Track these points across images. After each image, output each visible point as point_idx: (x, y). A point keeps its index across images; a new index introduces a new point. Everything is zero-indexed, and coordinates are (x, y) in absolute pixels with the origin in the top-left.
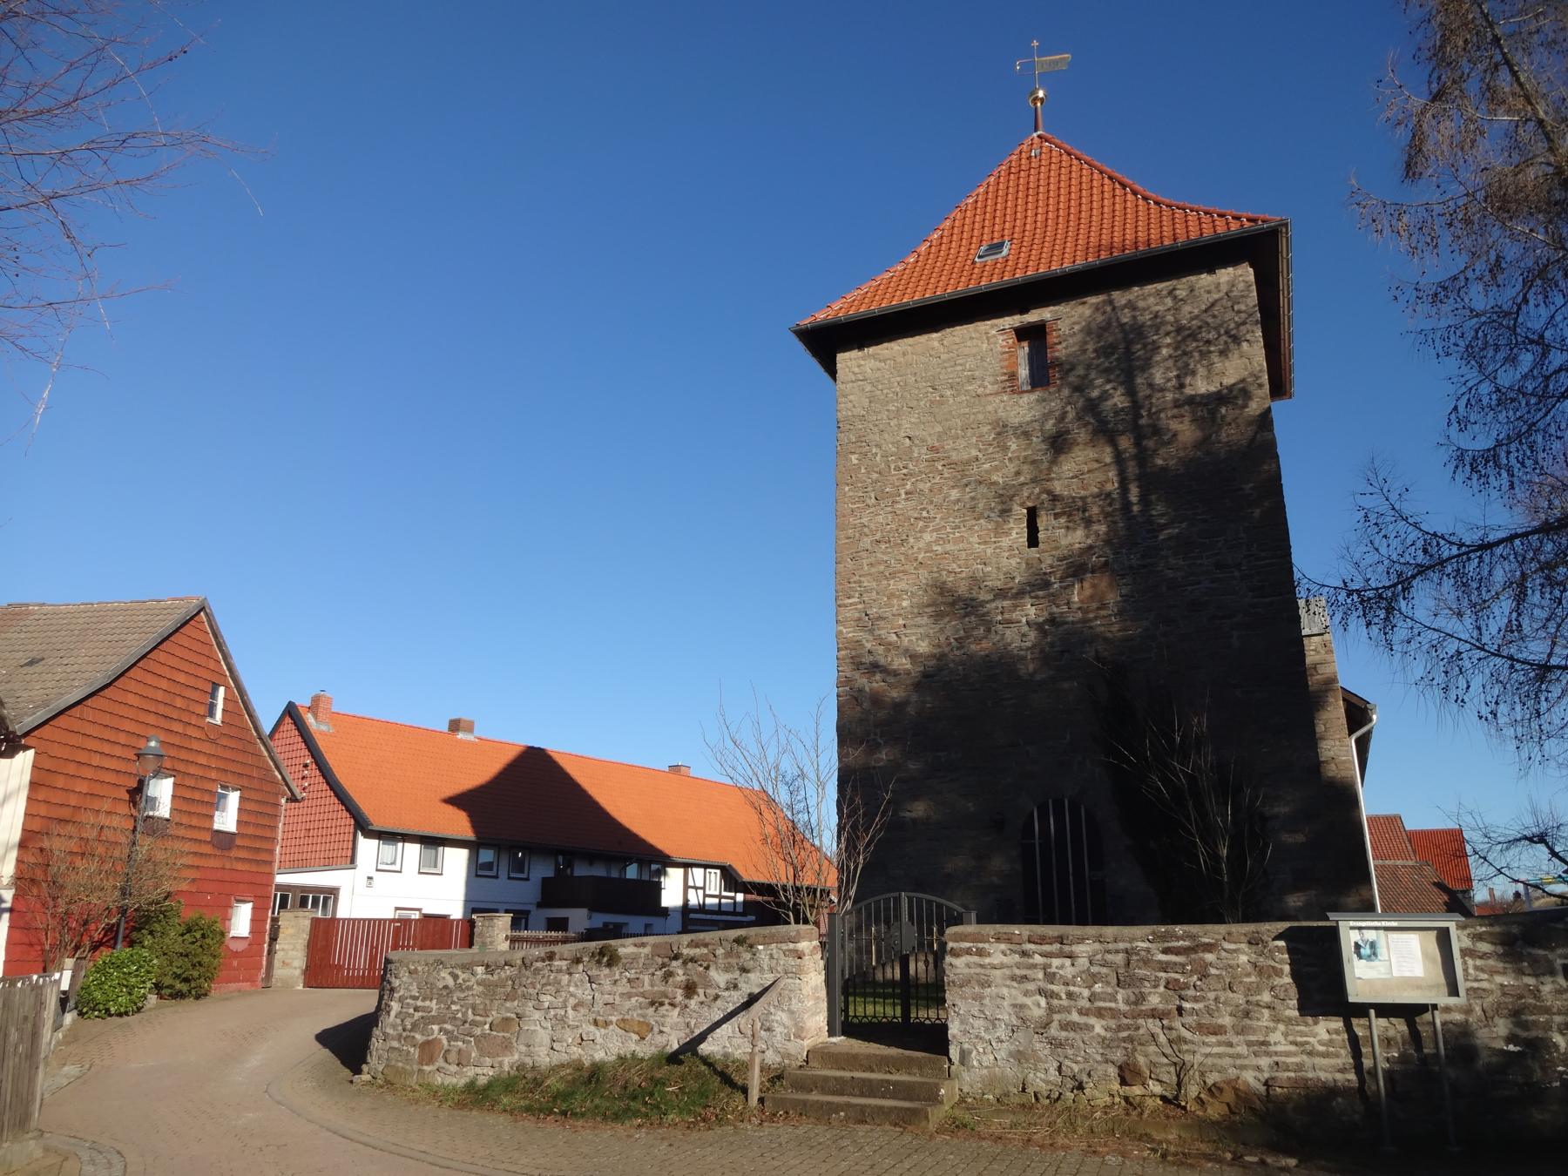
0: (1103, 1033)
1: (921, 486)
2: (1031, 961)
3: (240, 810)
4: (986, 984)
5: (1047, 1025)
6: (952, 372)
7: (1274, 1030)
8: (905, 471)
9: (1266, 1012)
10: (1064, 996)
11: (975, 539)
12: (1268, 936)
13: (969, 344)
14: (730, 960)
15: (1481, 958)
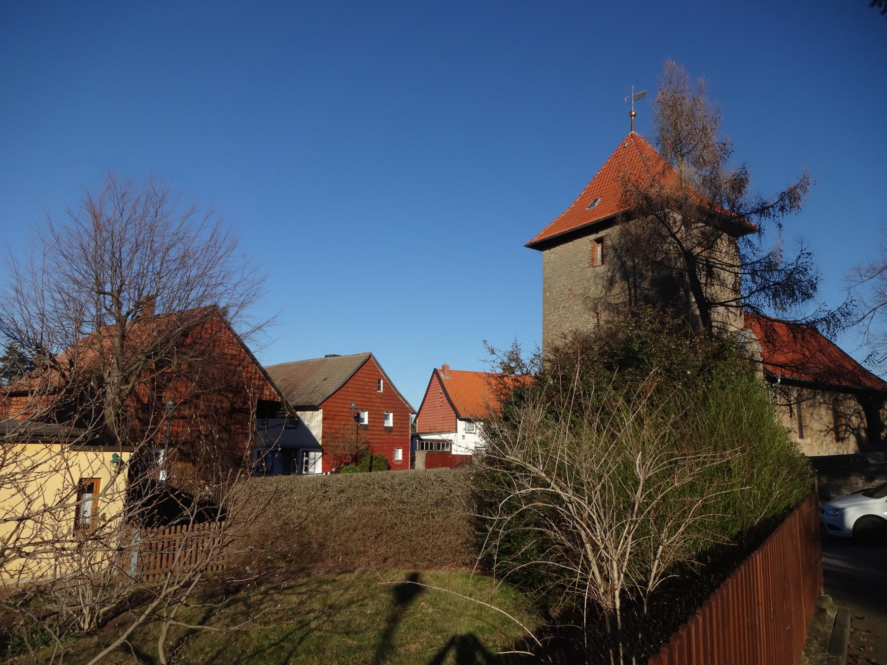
3: (369, 417)
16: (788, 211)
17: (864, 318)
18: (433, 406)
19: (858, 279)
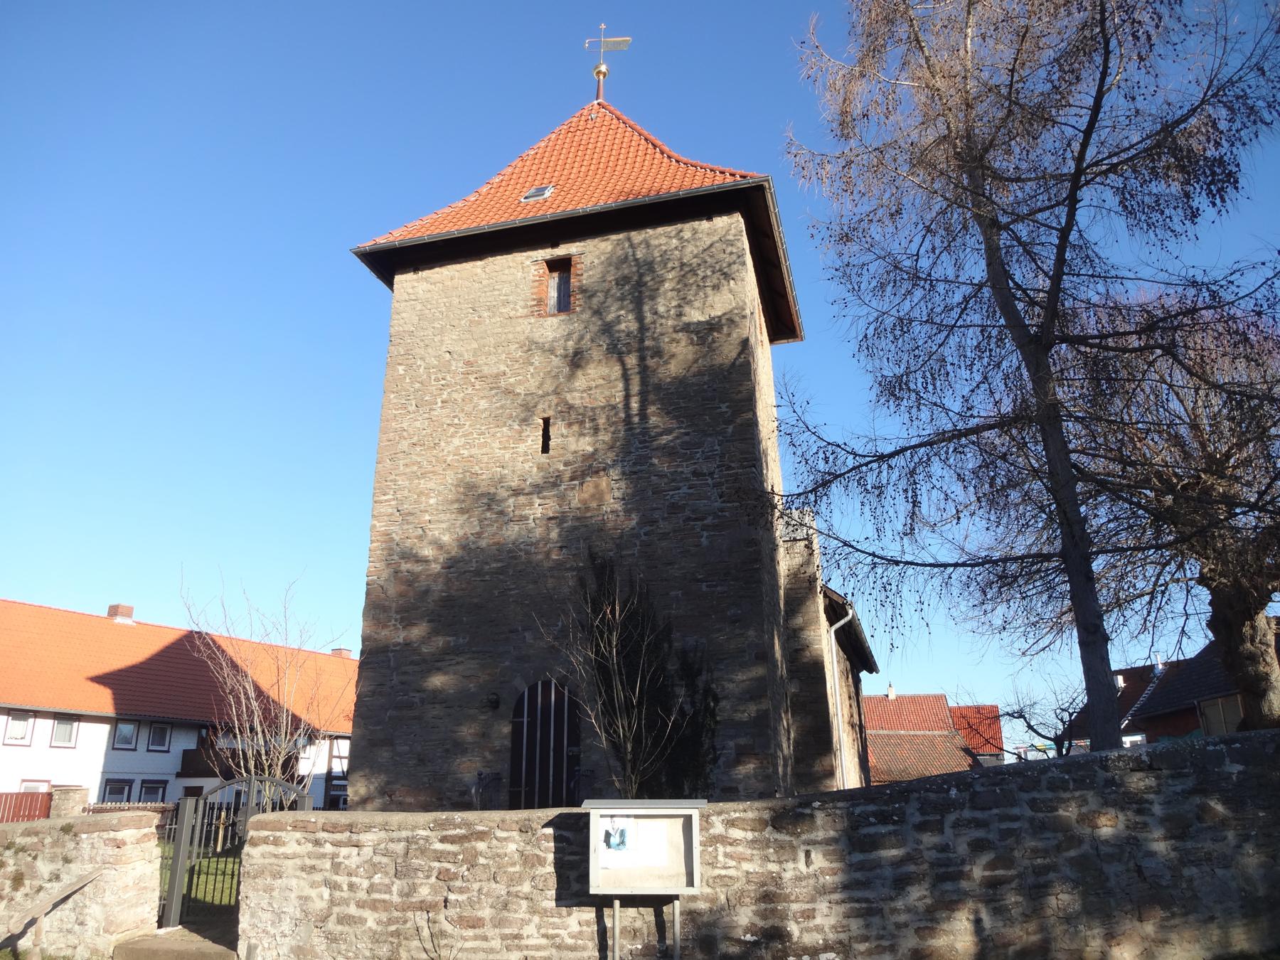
0: (374, 926)
1: (455, 395)
2: (322, 850)
4: (278, 875)
5: (325, 919)
6: (491, 296)
7: (528, 922)
8: (443, 382)
9: (524, 904)
10: (345, 887)
11: (497, 445)
12: (538, 823)
13: (506, 272)
14: (55, 850)
15: (731, 844)
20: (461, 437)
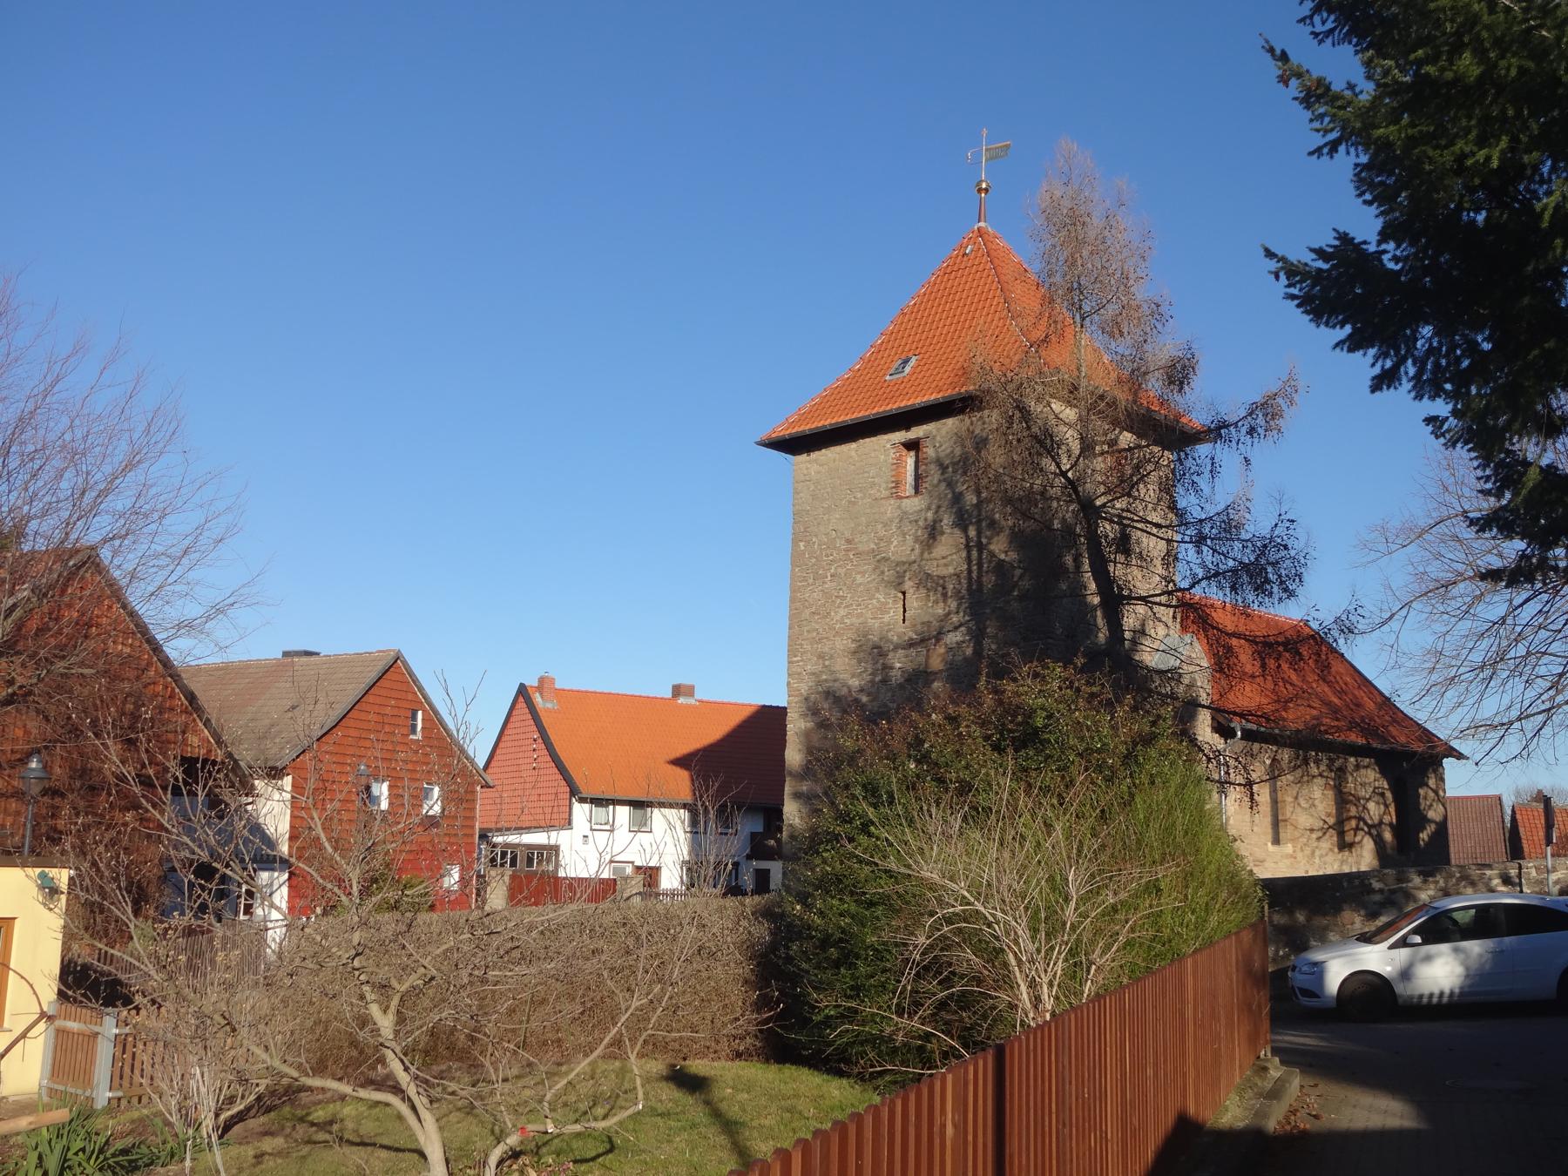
16: (1262, 437)
17: (1391, 618)
18: (514, 768)
19: (1383, 547)
20: (845, 607)
